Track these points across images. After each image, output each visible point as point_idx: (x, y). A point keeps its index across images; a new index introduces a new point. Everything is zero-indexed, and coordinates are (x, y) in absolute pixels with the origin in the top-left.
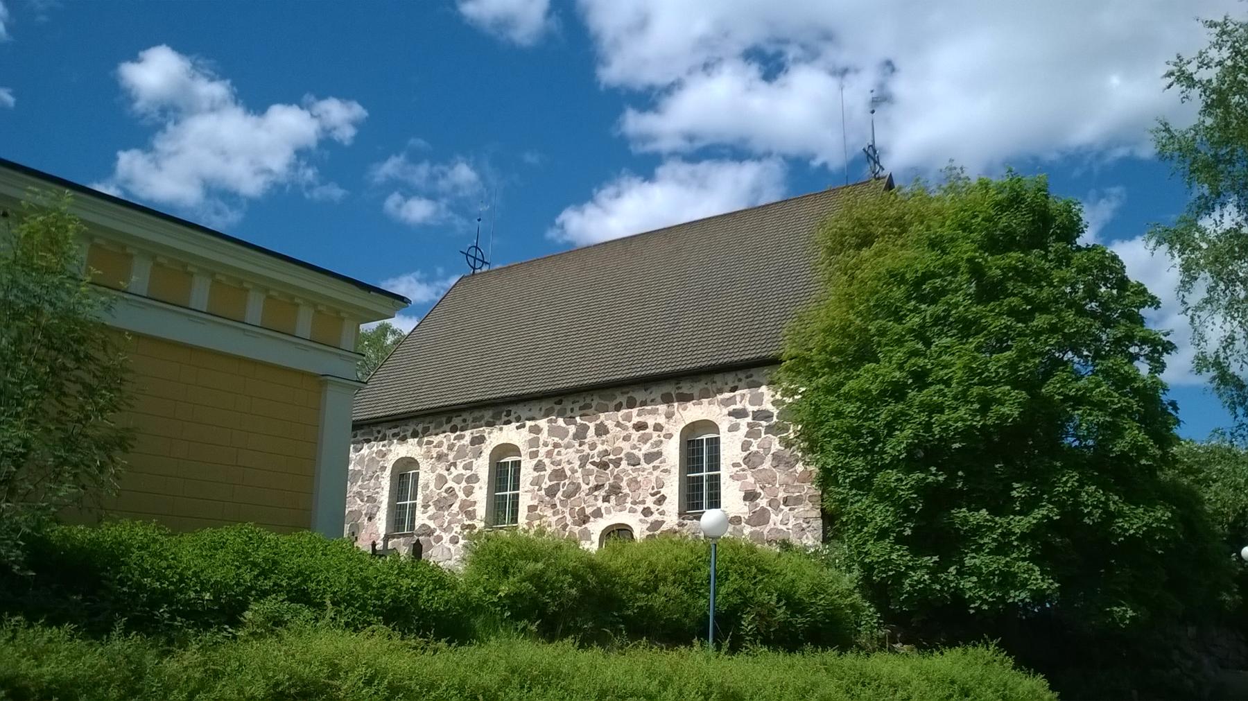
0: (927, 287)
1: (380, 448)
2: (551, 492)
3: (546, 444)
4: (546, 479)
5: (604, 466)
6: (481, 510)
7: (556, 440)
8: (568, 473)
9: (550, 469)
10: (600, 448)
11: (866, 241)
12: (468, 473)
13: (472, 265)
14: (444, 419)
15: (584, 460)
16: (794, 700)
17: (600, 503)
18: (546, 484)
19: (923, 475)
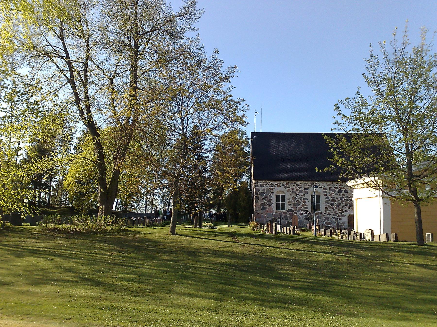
0: (205, 125)
1: (271, 187)
2: (332, 205)
3: (329, 193)
4: (330, 201)
5: (347, 200)
6: (309, 207)
7: (332, 192)
8: (337, 201)
9: (331, 199)
10: (346, 196)
11: (247, 312)
12: (304, 197)
13: (54, 47)
14: (293, 182)
15: (341, 198)
16: (436, 146)
17: (347, 209)
18: (330, 202)
19: (431, 114)
